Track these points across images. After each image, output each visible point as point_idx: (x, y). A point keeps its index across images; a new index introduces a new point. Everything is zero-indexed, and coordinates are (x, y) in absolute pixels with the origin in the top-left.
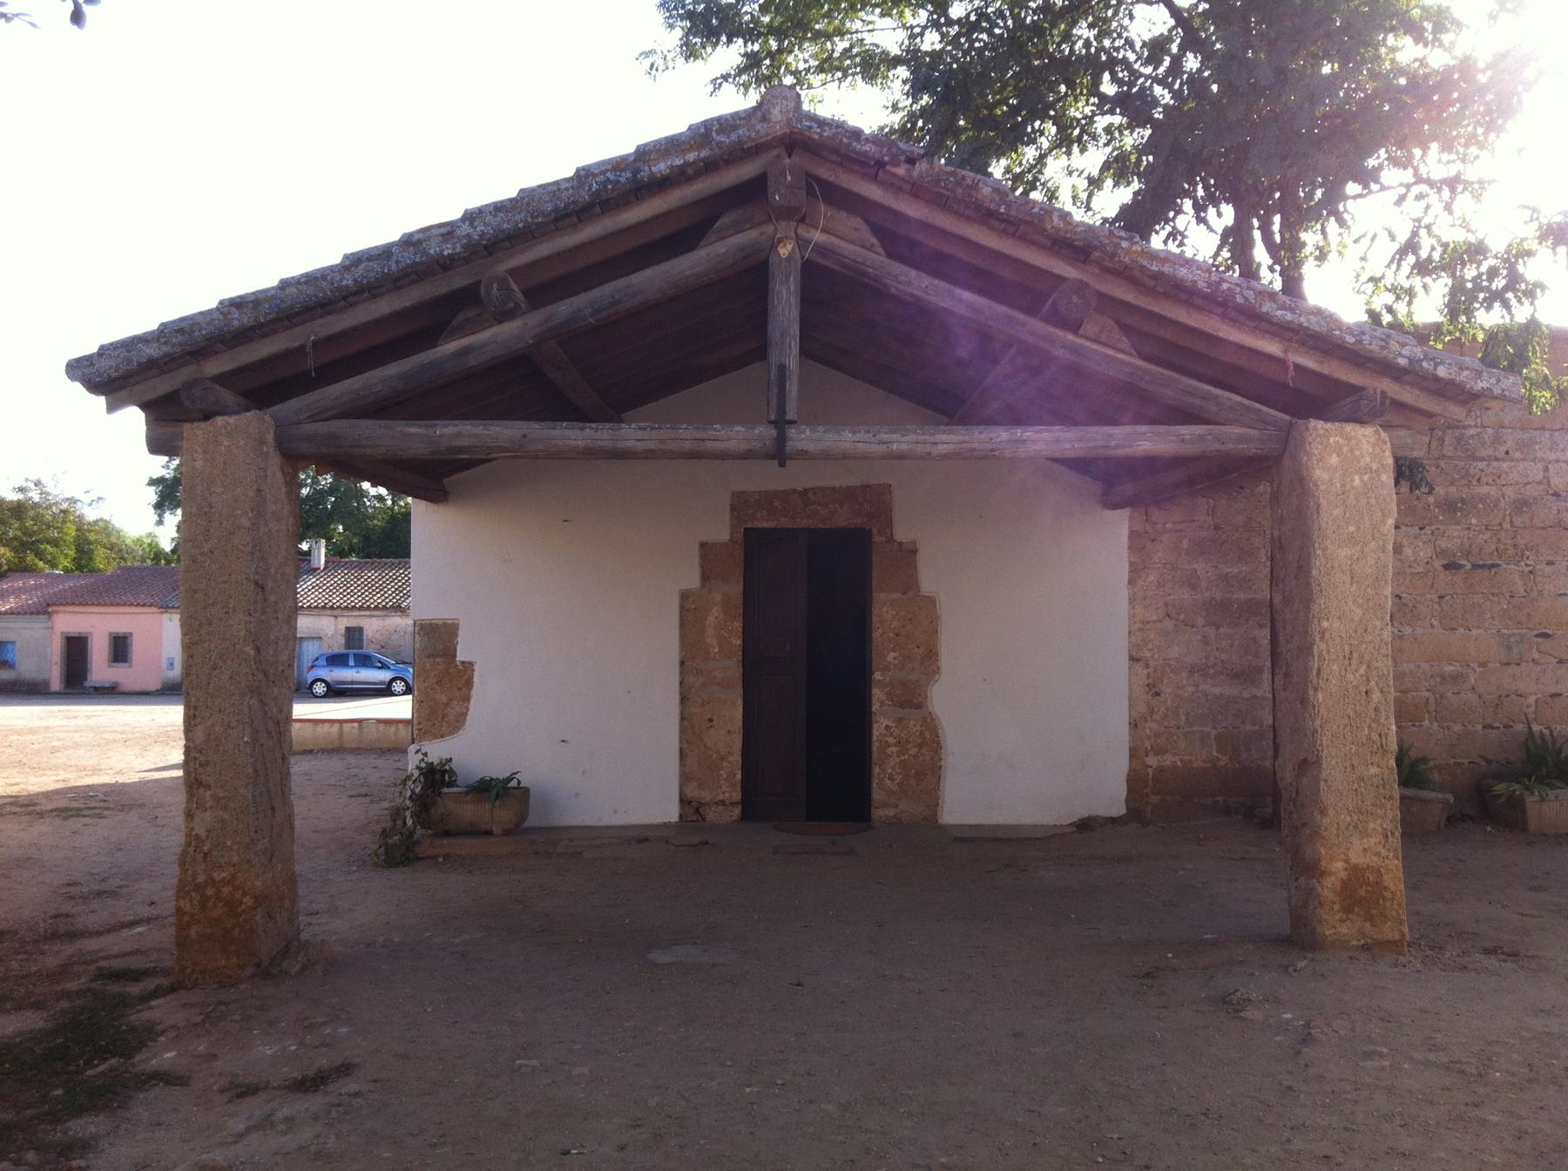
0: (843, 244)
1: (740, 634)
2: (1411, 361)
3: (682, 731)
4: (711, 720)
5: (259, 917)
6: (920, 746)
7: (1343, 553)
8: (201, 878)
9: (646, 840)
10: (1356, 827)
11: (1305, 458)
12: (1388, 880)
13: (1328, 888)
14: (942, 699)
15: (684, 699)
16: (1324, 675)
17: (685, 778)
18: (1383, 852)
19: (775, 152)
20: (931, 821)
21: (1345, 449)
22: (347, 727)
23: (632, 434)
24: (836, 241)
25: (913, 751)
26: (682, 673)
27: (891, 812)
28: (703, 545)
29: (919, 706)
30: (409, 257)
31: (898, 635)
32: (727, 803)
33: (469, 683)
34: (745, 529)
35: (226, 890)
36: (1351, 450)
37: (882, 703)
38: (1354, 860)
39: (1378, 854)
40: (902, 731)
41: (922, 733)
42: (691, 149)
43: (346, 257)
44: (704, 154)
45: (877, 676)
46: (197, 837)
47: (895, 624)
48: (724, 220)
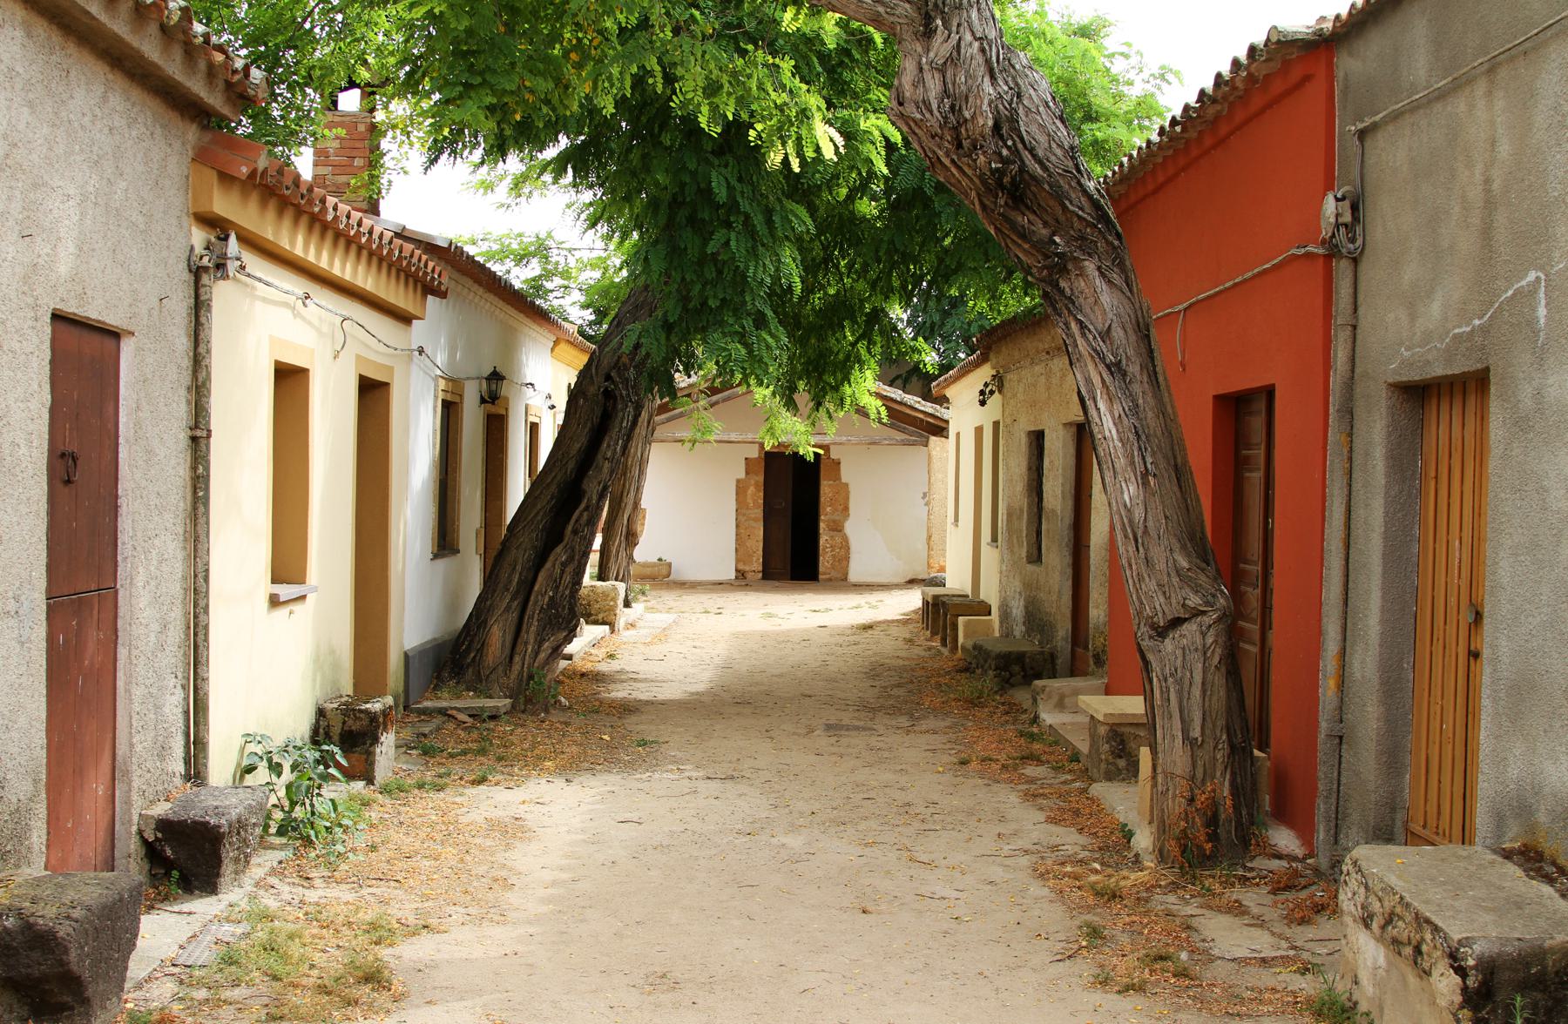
17: (738, 561)
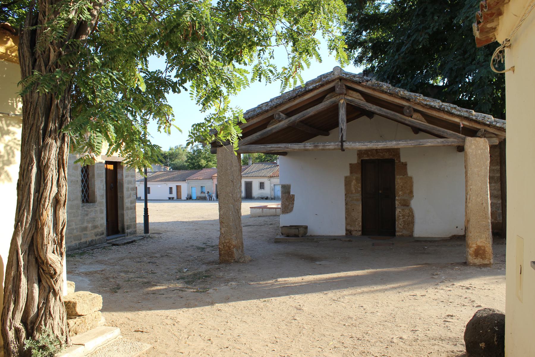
0: (355, 100)
2: (490, 122)
3: (346, 212)
5: (234, 250)
6: (408, 216)
7: (476, 170)
8: (223, 242)
9: (335, 239)
12: (487, 249)
13: (471, 250)
14: (414, 204)
15: (346, 204)
16: (471, 199)
17: (347, 224)
19: (337, 81)
21: (476, 144)
22: (277, 210)
23: (309, 145)
24: (353, 99)
25: (407, 218)
27: (401, 234)
28: (350, 164)
29: (408, 206)
30: (259, 111)
33: (294, 200)
37: (398, 205)
39: (484, 243)
41: (409, 213)
42: (317, 83)
43: (247, 111)
44: (320, 83)
45: (397, 198)
46: (222, 233)
47: (401, 184)
48: (328, 96)
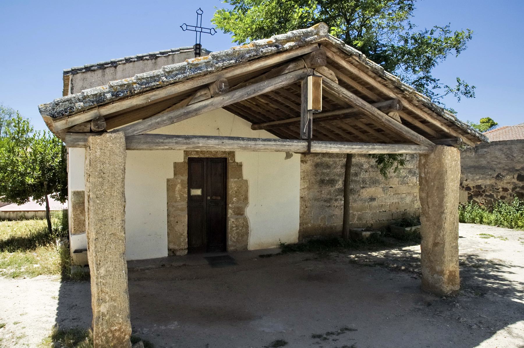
1: (187, 193)
4: (177, 222)
10: (451, 260)
11: (444, 157)
14: (250, 212)
17: (169, 242)
18: (456, 266)
20: (245, 249)
25: (240, 229)
26: (168, 206)
29: (242, 215)
31: (236, 192)
32: (183, 249)
34: (188, 158)
35: (117, 334)
36: (453, 154)
38: (450, 270)
40: (237, 223)
45: (230, 205)
